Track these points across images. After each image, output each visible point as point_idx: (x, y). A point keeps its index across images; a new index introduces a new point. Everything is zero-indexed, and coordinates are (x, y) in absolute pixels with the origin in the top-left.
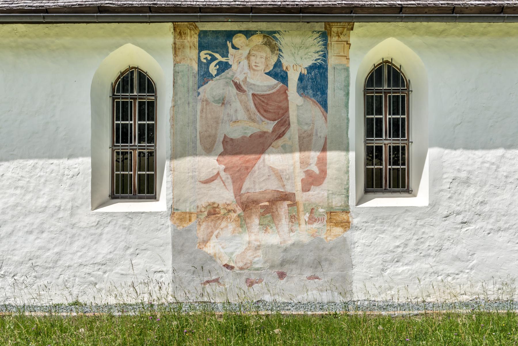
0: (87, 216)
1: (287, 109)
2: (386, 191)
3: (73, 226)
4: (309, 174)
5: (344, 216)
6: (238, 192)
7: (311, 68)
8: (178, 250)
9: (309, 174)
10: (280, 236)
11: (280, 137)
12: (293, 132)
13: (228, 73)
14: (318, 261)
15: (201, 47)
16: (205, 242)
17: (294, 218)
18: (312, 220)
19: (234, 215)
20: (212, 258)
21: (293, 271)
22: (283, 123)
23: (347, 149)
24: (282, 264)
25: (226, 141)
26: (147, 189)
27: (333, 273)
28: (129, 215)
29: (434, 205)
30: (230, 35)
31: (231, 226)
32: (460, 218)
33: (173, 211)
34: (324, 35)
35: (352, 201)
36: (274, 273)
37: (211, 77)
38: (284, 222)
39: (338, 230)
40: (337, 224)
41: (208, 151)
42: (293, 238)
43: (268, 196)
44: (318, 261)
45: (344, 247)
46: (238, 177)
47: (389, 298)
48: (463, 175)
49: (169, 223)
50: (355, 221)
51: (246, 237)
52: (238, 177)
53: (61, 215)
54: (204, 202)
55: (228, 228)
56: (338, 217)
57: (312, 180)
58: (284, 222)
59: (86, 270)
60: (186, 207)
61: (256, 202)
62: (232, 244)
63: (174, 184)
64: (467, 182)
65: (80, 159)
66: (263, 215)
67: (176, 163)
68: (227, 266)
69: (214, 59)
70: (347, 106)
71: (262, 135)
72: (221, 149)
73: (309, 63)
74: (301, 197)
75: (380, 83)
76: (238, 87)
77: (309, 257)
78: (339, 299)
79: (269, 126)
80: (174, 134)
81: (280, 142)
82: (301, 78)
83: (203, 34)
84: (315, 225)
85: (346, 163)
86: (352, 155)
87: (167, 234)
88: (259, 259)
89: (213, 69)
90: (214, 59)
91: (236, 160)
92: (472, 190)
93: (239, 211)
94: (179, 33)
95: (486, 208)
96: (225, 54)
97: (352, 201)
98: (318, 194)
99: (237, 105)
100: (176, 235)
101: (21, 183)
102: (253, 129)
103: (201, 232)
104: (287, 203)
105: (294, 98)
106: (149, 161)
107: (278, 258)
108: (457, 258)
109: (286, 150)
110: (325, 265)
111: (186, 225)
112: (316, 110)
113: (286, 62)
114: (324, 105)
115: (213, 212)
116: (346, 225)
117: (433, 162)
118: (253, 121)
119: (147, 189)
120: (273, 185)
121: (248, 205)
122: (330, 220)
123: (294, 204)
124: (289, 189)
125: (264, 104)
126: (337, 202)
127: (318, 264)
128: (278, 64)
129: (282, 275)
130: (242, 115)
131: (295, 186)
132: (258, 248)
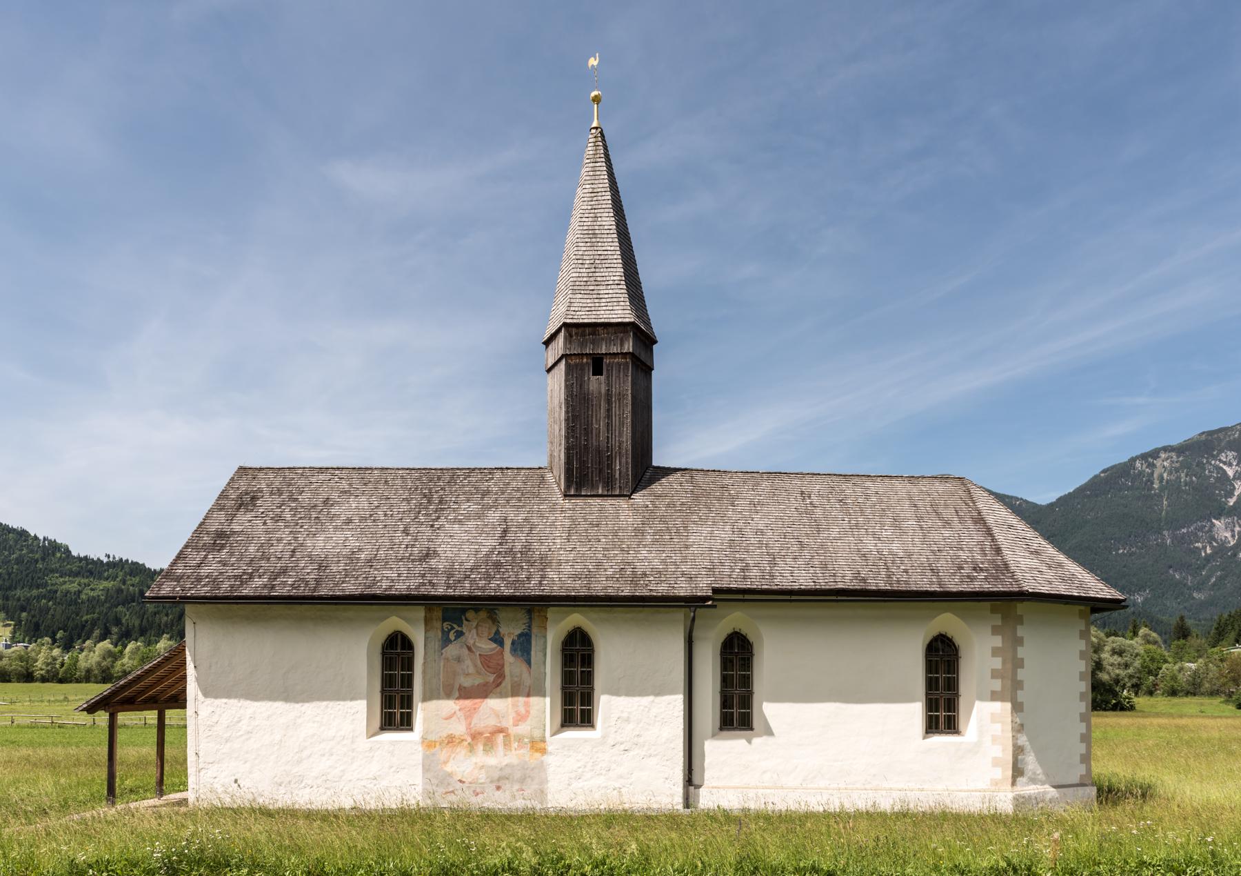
0: (364, 743)
1: (503, 666)
2: (577, 726)
3: (353, 750)
4: (518, 713)
5: (542, 745)
6: (469, 727)
7: (520, 636)
8: (426, 769)
9: (518, 713)
10: (499, 758)
11: (498, 685)
12: (507, 683)
13: (463, 639)
14: (525, 776)
15: (444, 620)
16: (445, 763)
17: (507, 745)
18: (520, 747)
19: (465, 743)
20: (450, 775)
21: (506, 785)
22: (501, 676)
23: (544, 696)
24: (498, 780)
25: (461, 688)
26: (406, 723)
27: (535, 786)
28: (393, 743)
29: (604, 737)
30: (464, 611)
31: (463, 752)
32: (622, 747)
33: (424, 739)
34: (530, 612)
35: (548, 733)
36: (493, 786)
37: (450, 641)
38: (501, 748)
39: (538, 755)
40: (537, 751)
41: (448, 696)
42: (506, 761)
43: (490, 730)
44: (525, 776)
45: (542, 767)
46: (469, 715)
47: (993, 862)
48: (625, 715)
49: (420, 749)
50: (550, 748)
51: (474, 759)
52: (469, 715)
53: (345, 742)
54: (444, 734)
55: (462, 752)
56: (538, 745)
57: (521, 718)
58: (501, 748)
59: (363, 783)
60: (432, 737)
61: (481, 734)
62: (467, 766)
63: (425, 720)
64: (628, 720)
65: (359, 702)
66: (485, 745)
67: (434, 704)
68: (460, 781)
69: (453, 628)
70: (544, 663)
71: (485, 684)
72: (457, 695)
73: (518, 632)
74: (513, 731)
75: (732, 647)
76: (469, 649)
77: (518, 775)
78: (538, 807)
79: (491, 678)
80: (424, 684)
81: (498, 689)
82: (513, 643)
83: (445, 611)
84: (522, 751)
85: (545, 707)
86: (548, 700)
87: (419, 757)
88: (482, 777)
89: (452, 636)
90: (453, 628)
91: (468, 703)
92: (631, 726)
93: (469, 740)
94: (429, 609)
95: (641, 740)
96: (460, 625)
97: (548, 733)
98: (523, 729)
99: (468, 662)
100: (426, 757)
101: (318, 719)
102: (478, 681)
103: (443, 755)
104: (501, 735)
105: (508, 657)
106: (408, 702)
107: (496, 775)
108: (621, 777)
109: (503, 695)
110: (529, 780)
111: (433, 750)
112: (524, 667)
113: (504, 630)
114: (529, 663)
115: (451, 740)
116: (543, 751)
117: (606, 705)
118: (479, 673)
119: (406, 723)
120: (492, 722)
121: (475, 736)
122: (532, 747)
123: (507, 736)
124: (504, 724)
125: (486, 660)
126: (537, 734)
127: (522, 780)
128: (497, 632)
129: (498, 788)
130: (471, 670)
131: (508, 723)
132: (482, 767)
